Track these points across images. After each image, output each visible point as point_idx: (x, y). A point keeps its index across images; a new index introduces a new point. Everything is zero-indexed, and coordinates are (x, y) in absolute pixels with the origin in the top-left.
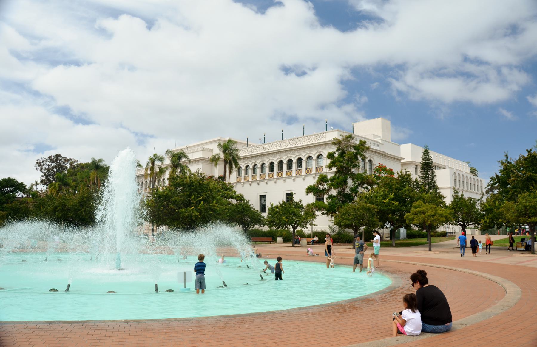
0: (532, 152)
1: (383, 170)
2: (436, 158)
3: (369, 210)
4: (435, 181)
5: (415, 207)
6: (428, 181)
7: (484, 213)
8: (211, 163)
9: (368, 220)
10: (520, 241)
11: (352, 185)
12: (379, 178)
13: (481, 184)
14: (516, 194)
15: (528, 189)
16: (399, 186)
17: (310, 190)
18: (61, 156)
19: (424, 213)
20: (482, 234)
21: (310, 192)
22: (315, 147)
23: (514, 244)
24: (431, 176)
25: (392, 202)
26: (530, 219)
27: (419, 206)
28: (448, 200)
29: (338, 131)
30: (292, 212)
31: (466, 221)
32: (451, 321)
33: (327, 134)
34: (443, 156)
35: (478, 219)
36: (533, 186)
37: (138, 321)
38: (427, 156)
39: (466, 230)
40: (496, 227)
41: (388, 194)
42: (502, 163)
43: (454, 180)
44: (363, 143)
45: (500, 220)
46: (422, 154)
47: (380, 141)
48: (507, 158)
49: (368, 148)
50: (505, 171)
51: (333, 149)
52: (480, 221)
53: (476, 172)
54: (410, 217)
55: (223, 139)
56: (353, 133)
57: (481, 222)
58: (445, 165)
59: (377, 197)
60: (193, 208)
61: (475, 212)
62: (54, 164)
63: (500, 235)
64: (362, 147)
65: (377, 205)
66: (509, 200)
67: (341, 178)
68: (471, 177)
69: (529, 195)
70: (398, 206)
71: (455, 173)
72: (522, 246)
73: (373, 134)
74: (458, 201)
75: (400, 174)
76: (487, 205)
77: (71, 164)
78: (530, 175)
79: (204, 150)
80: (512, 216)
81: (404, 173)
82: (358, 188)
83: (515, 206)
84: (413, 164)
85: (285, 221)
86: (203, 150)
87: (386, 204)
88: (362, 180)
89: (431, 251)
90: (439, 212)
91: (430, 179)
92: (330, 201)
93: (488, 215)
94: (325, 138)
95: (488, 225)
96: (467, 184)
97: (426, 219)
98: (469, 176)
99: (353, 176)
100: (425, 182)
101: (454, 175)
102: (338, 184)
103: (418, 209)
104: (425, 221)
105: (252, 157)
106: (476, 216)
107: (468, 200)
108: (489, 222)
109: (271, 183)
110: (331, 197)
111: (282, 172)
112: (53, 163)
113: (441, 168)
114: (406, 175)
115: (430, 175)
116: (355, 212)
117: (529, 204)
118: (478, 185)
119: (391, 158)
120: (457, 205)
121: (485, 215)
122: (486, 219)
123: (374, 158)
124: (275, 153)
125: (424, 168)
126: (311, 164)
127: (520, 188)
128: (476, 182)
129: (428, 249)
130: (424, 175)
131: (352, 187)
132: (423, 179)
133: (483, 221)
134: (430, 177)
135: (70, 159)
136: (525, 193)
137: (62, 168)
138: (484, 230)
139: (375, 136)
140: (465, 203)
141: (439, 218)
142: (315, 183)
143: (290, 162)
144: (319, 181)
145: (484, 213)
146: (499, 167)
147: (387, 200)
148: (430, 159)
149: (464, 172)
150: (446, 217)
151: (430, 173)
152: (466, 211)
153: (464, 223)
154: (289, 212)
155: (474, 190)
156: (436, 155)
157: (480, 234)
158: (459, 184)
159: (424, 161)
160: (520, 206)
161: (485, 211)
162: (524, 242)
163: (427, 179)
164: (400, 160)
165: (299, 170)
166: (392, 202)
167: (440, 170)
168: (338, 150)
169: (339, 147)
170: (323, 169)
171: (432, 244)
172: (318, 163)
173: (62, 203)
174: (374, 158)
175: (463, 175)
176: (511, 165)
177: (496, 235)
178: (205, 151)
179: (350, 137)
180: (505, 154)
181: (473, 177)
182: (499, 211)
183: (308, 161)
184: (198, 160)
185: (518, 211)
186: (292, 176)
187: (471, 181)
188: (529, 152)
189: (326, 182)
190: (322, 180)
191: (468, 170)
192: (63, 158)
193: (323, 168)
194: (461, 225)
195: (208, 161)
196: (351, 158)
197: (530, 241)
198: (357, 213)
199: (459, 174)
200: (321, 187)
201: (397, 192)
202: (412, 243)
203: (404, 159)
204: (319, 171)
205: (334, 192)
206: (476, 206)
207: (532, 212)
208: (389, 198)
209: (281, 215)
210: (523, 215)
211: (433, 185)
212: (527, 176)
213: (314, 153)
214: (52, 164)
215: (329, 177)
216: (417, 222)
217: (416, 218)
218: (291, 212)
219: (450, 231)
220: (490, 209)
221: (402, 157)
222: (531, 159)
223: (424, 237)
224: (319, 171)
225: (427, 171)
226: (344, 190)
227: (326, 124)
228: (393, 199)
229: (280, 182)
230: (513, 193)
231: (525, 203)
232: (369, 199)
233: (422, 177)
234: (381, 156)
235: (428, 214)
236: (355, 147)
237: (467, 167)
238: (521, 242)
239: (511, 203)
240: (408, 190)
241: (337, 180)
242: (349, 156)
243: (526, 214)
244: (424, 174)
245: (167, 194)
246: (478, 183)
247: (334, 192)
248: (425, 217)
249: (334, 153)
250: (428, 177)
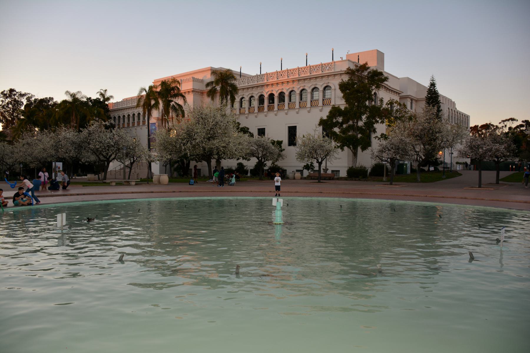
8: (201, 94)
18: (15, 91)
37: (408, 182)
51: (346, 78)
56: (358, 62)
62: (9, 100)
77: (28, 99)
89: (481, 187)
109: (271, 114)
111: (263, 106)
112: (7, 98)
135: (26, 93)
137: (17, 103)
143: (271, 96)
146: (449, 108)
165: (271, 105)
170: (330, 101)
183: (313, 93)
186: (264, 111)
192: (17, 92)
193: (306, 103)
197: (441, 167)
204: (327, 103)
214: (6, 100)
224: (327, 103)
229: (282, 114)
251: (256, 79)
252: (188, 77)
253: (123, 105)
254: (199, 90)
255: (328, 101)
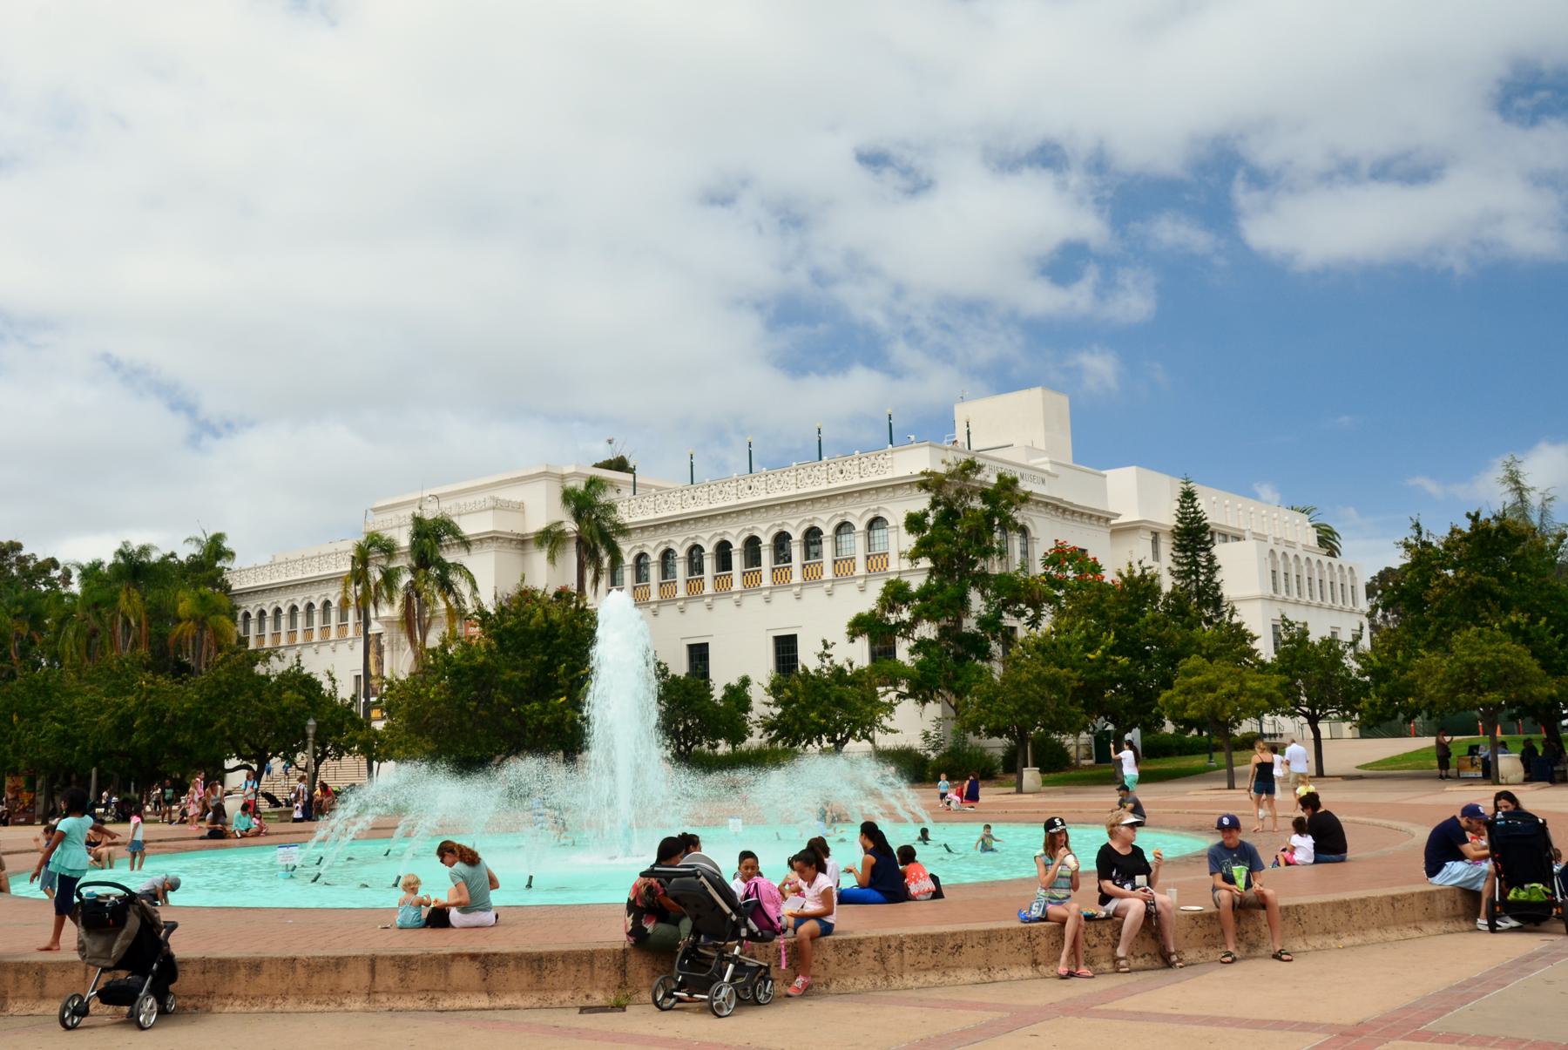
0: (1482, 518)
1: (1071, 561)
2: (1215, 508)
3: (1053, 684)
4: (1217, 584)
5: (1188, 674)
6: (1197, 585)
7: (1367, 678)
8: (519, 546)
9: (1056, 713)
10: (1466, 752)
11: (983, 608)
12: (1057, 583)
13: (1353, 579)
14: (1445, 629)
15: (1476, 620)
16: (1125, 610)
17: (860, 626)
19: (1211, 688)
20: (1362, 737)
21: (861, 633)
22: (860, 496)
23: (1453, 760)
24: (1205, 571)
25: (1112, 657)
26: (1484, 696)
27: (1195, 672)
28: (1265, 649)
29: (930, 445)
30: (836, 698)
31: (1319, 702)
32: (1346, 852)
33: (895, 455)
34: (1236, 497)
35: (1353, 698)
36: (1488, 609)
38: (1192, 510)
39: (1319, 726)
40: (1401, 716)
41: (1097, 636)
42: (1407, 546)
43: (1270, 572)
44: (1007, 485)
45: (1411, 700)
46: (1177, 505)
47: (1047, 467)
48: (1420, 533)
49: (1026, 498)
50: (1416, 570)
51: (920, 502)
52: (1358, 702)
53: (1334, 540)
54: (1175, 702)
55: (555, 471)
57: (1361, 706)
58: (1243, 527)
59: (1068, 646)
60: (562, 699)
61: (1342, 678)
63: (1417, 736)
64: (1006, 493)
65: (1074, 669)
66: (1430, 646)
67: (950, 589)
68: (1323, 561)
69: (1480, 635)
70: (1129, 666)
71: (1272, 551)
72: (1473, 765)
73: (1027, 447)
74: (1294, 650)
75: (1126, 575)
76: (1374, 659)
78: (1480, 581)
79: (499, 506)
80: (1438, 691)
81: (1138, 573)
82: (1002, 617)
83: (1445, 663)
84: (1145, 528)
85: (818, 724)
86: (494, 508)
87: (1095, 664)
88: (1014, 593)
89: (1234, 788)
90: (1250, 684)
91: (1202, 578)
92: (920, 657)
93: (1377, 685)
94: (892, 467)
95: (1379, 712)
96: (1310, 584)
97: (1219, 704)
98: (1314, 558)
99: (982, 580)
100: (1187, 586)
101: (1269, 560)
102: (943, 608)
103: (1194, 680)
104: (1217, 710)
105: (657, 527)
106: (1346, 690)
107: (1321, 645)
108: (1383, 704)
109: (724, 605)
110: (922, 645)
111: (701, 579)
113: (1230, 539)
114: (1143, 577)
115: (1204, 567)
116: (1020, 692)
117: (1479, 658)
118: (1342, 585)
119: (1082, 514)
120: (1292, 662)
121: (1370, 687)
122: (1374, 697)
123: (1034, 519)
124: (733, 512)
125: (1185, 546)
126: (852, 545)
127: (1456, 614)
128: (1338, 575)
129: (1225, 785)
130: (1185, 568)
131: (985, 613)
132: (1183, 578)
133: (1364, 702)
134: (1203, 573)
136: (1468, 628)
138: (1370, 728)
139: (1031, 450)
140: (1315, 654)
141: (1252, 700)
142: (874, 608)
143: (752, 544)
144: (887, 600)
145: (1367, 678)
147: (1099, 652)
148: (1201, 519)
149: (1299, 547)
150: (1270, 697)
151: (1203, 561)
152: (1319, 676)
153: (1314, 711)
154: (826, 697)
155: (1333, 600)
156: (1214, 498)
157: (1358, 736)
158: (1287, 586)
159: (1180, 525)
160: (1458, 664)
161: (1371, 674)
162: (1477, 754)
163: (1193, 577)
164: (1108, 520)
166: (1112, 657)
167: (1225, 544)
168: (934, 504)
169: (937, 495)
171: (1235, 769)
172: (872, 542)
173: (151, 703)
174: (1035, 520)
175: (1296, 556)
176: (1430, 550)
177: (1406, 736)
178: (499, 509)
179: (971, 466)
180: (1411, 524)
181: (1326, 560)
182: (1404, 677)
183: (839, 538)
184: (480, 540)
185: (1451, 676)
187: (1321, 572)
188: (1475, 518)
189: (905, 603)
190: (895, 598)
191: (1312, 538)
194: (1305, 715)
195: (511, 540)
196: (978, 531)
198: (1026, 694)
199: (1284, 553)
200: (893, 618)
201: (1124, 628)
202: (1166, 770)
203: (1118, 515)
205: (927, 630)
206: (1344, 661)
207: (1487, 679)
208: (1103, 647)
209: (803, 708)
210: (1465, 686)
211: (1212, 596)
212: (1471, 583)
213: (858, 512)
215: (914, 588)
216: (1194, 712)
217: (1193, 704)
218: (833, 699)
219: (1267, 729)
220: (1382, 668)
221: (1112, 509)
222: (1477, 538)
223: (1193, 753)
225: (1194, 555)
226: (959, 622)
227: (890, 424)
228: (1113, 650)
229: (753, 602)
230: (1439, 629)
231: (1469, 655)
232: (1043, 649)
233: (1179, 572)
234: (1053, 513)
235: (1223, 691)
236: (986, 496)
237: (1307, 528)
238: (1469, 755)
239: (1436, 655)
240: (1154, 621)
241: (939, 596)
242: (972, 523)
243: (1472, 684)
244: (1183, 564)
245: (484, 663)
246: (1343, 577)
247: (927, 630)
248: (1216, 699)
249: (926, 514)
250: (1197, 573)
251: (857, 470)
252: (480, 497)
253: (309, 569)
254: (514, 534)
255: (846, 565)
